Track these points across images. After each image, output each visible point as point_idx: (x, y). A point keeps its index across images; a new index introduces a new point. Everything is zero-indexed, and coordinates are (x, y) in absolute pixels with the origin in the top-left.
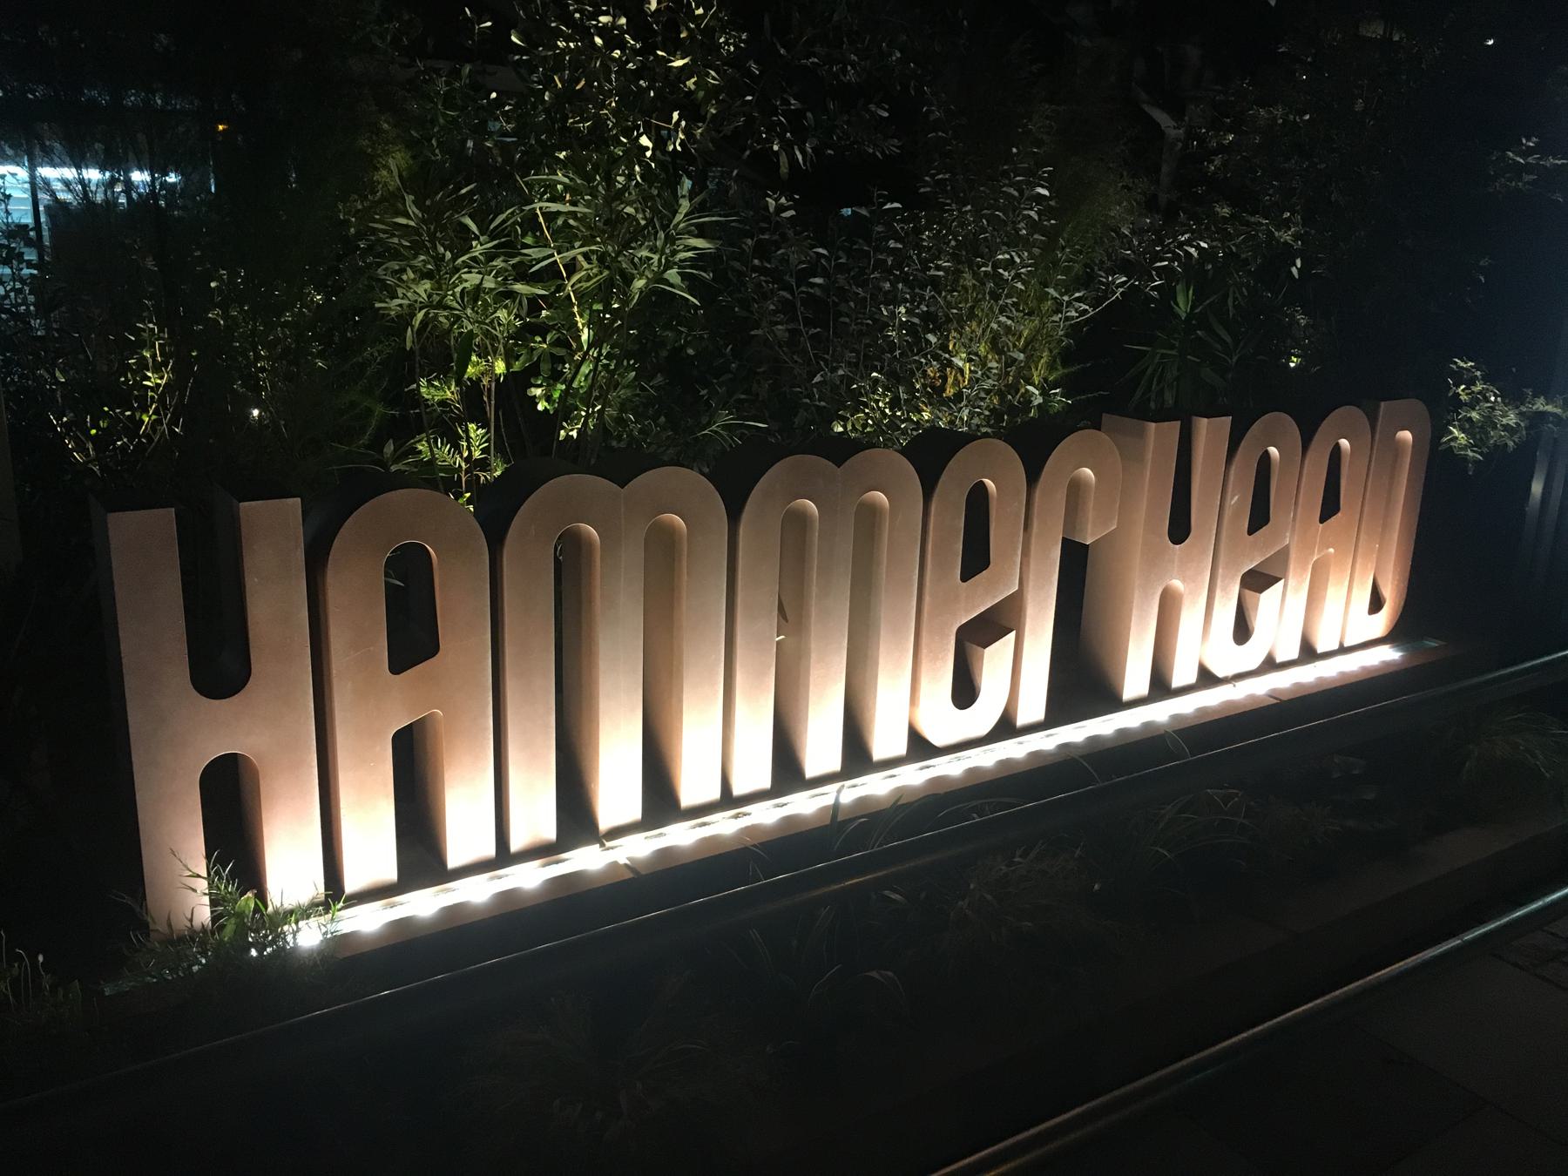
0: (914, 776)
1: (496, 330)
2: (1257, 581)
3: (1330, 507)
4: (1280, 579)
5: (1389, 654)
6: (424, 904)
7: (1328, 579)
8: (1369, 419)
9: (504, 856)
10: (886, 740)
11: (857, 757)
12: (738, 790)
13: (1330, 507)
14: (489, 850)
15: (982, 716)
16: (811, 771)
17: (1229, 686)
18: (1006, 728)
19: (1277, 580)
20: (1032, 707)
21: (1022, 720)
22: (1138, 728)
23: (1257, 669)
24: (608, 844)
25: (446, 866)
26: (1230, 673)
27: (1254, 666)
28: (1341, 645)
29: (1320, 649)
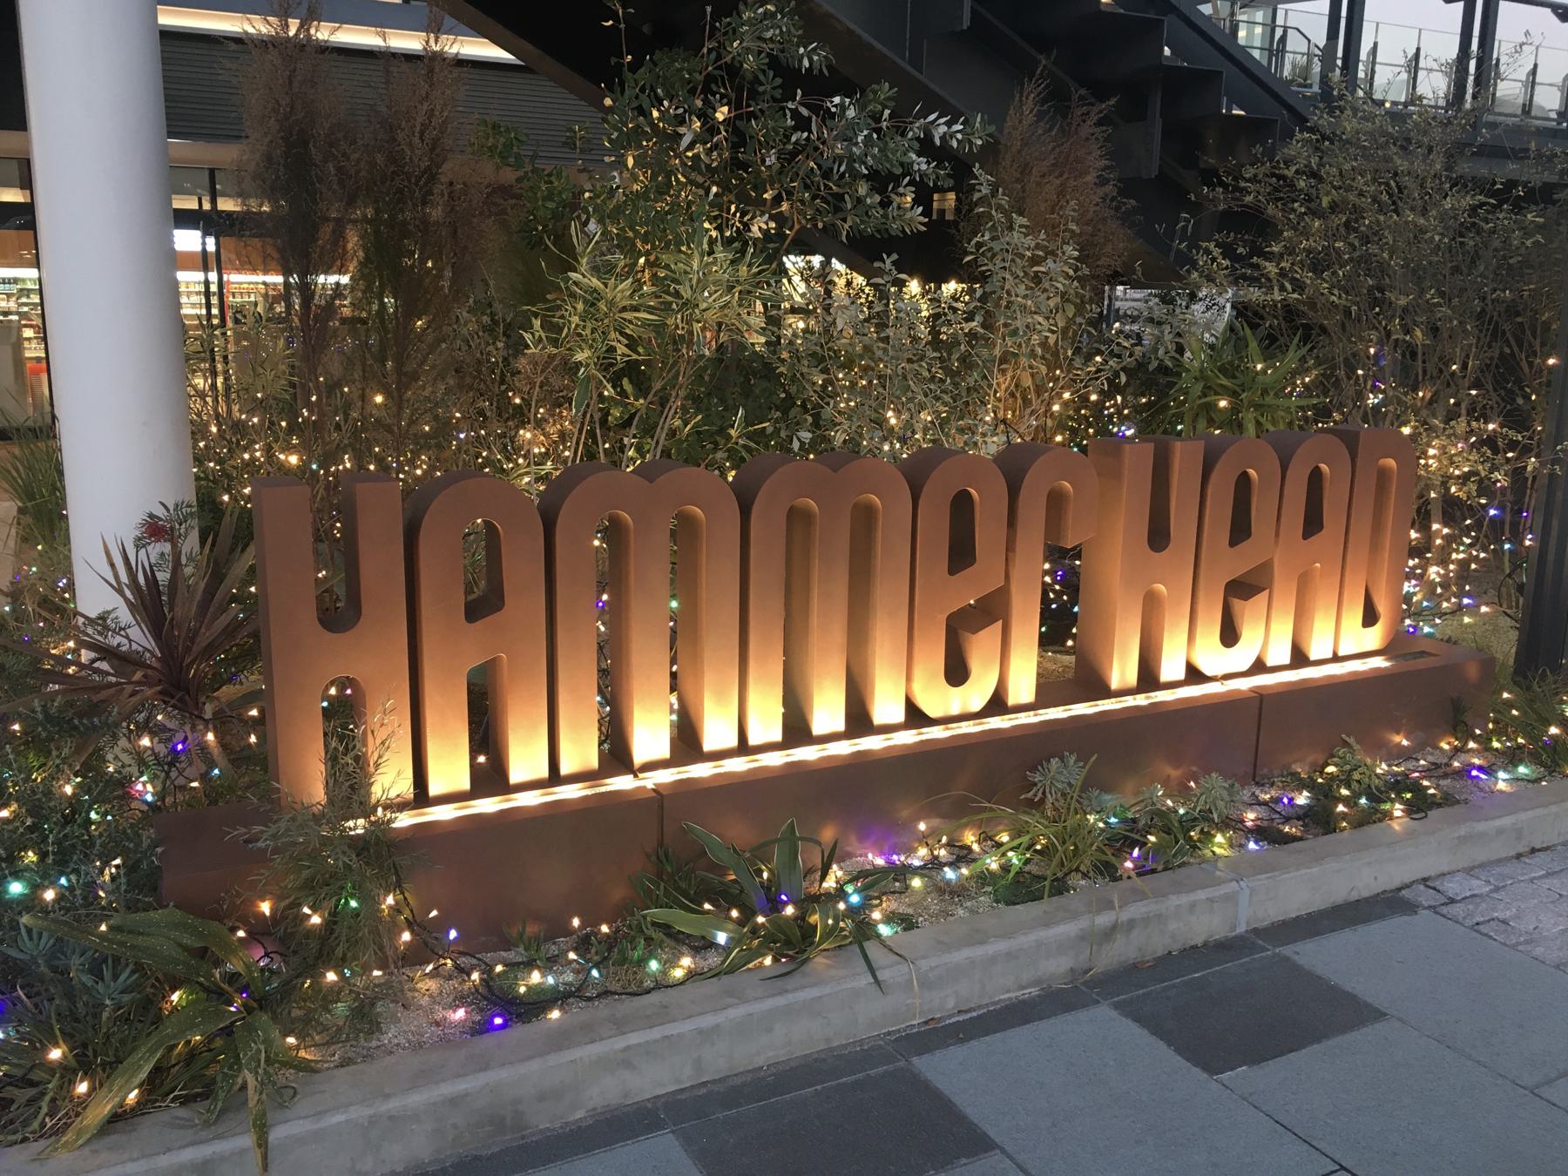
0: (908, 737)
1: (1237, 206)
2: (1242, 588)
3: (1313, 524)
4: (1264, 589)
5: (1380, 662)
6: (488, 805)
7: (703, 672)
8: (944, 460)
9: (555, 777)
10: (1171, 669)
11: (1148, 679)
12: (753, 740)
13: (1313, 524)
14: (543, 772)
15: (975, 694)
16: (708, 745)
17: (1218, 683)
18: (1259, 667)
19: (1260, 590)
20: (1022, 688)
21: (1013, 699)
22: (879, 750)
23: (978, 713)
24: (641, 775)
25: (559, 773)
26: (1220, 673)
27: (1245, 667)
28: (1335, 654)
29: (1313, 657)
